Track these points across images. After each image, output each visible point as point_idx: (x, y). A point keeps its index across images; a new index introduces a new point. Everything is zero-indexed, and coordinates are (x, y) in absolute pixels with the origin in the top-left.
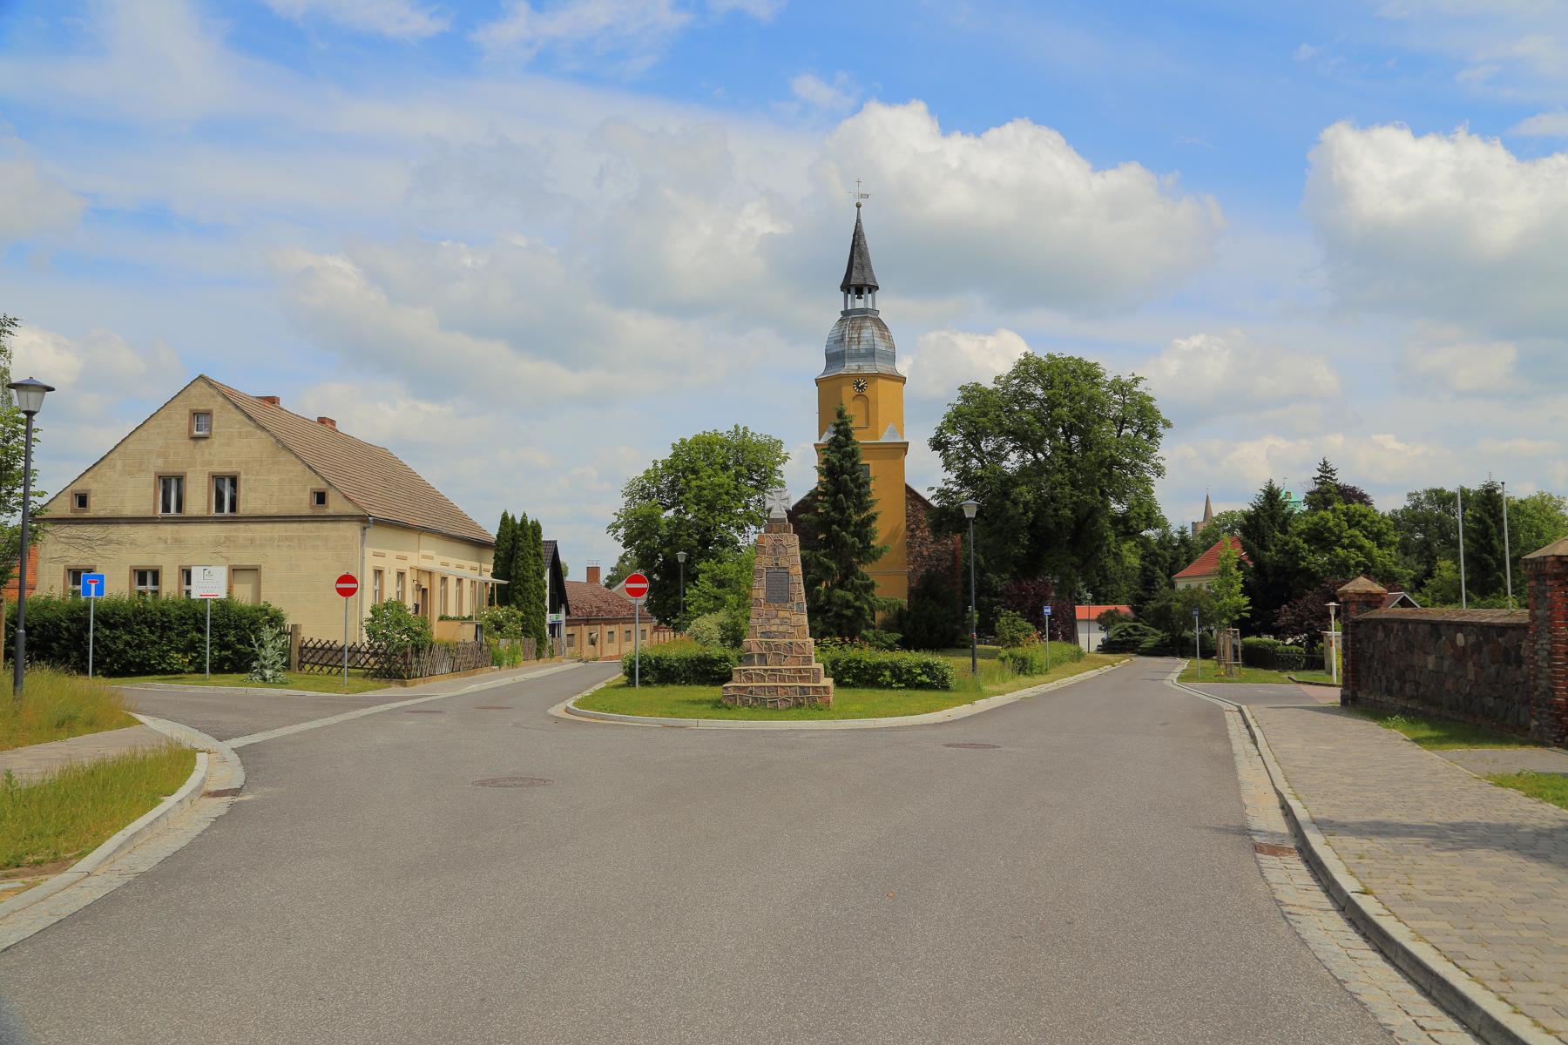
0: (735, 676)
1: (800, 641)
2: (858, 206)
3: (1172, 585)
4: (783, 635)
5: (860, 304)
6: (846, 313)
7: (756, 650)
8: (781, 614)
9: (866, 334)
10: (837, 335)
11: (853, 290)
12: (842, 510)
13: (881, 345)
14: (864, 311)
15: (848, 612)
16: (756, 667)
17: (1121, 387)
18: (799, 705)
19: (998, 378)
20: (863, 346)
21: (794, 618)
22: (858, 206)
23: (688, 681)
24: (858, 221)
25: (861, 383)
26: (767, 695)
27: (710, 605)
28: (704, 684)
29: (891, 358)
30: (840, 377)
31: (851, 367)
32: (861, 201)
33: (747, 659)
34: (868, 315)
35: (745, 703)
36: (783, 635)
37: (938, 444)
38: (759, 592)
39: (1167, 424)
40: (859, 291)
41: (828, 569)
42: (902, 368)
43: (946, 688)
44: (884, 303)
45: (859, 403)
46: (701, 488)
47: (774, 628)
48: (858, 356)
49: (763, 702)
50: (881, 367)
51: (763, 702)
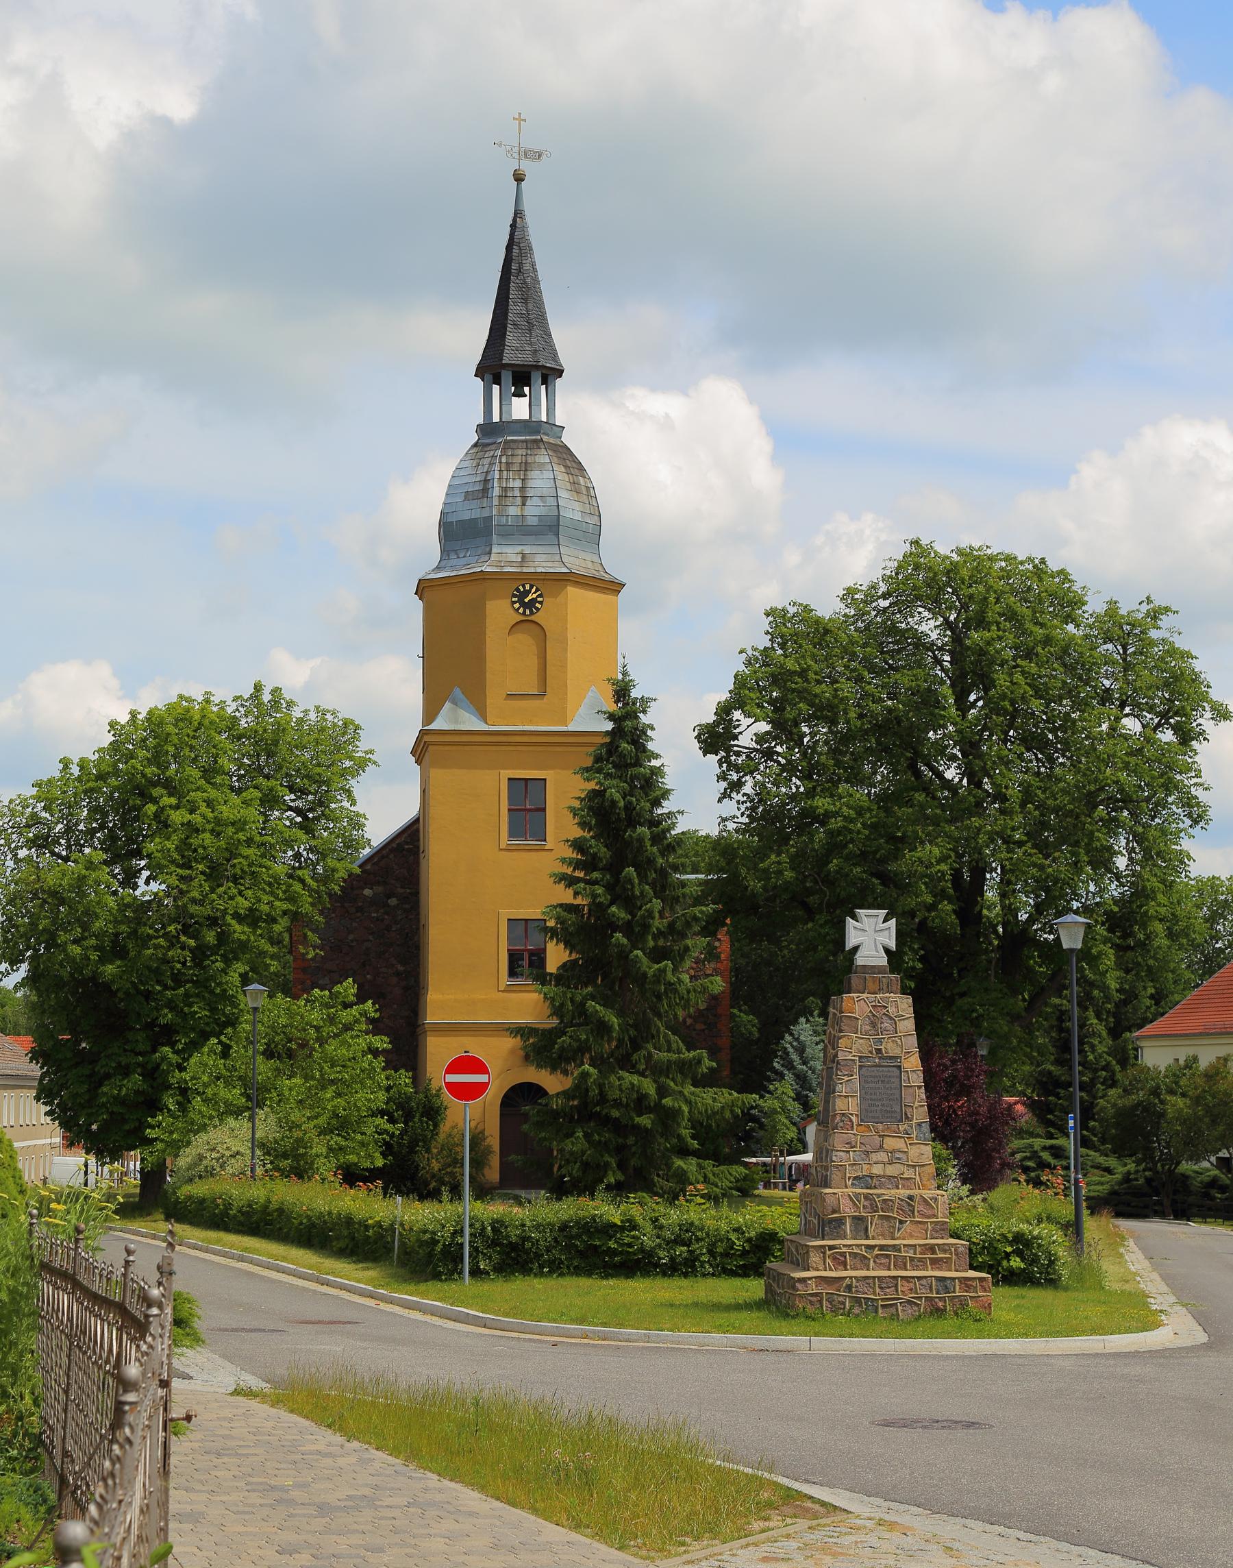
0: (815, 1258)
1: (927, 1194)
2: (519, 178)
3: (1126, 1057)
4: (895, 1181)
5: (520, 408)
6: (488, 430)
7: (848, 1210)
8: (890, 1143)
9: (540, 481)
10: (473, 481)
11: (507, 377)
12: (629, 903)
13: (572, 510)
14: (530, 426)
15: (645, 1121)
16: (848, 1242)
17: (1115, 627)
18: (938, 1312)
19: (850, 592)
20: (533, 510)
21: (914, 1152)
22: (519, 178)
23: (555, 1269)
24: (518, 214)
26: (878, 1294)
28: (589, 1274)
29: (592, 536)
30: (482, 577)
31: (505, 556)
32: (527, 166)
33: (829, 1225)
34: (539, 435)
35: (837, 1308)
36: (895, 1181)
37: (715, 738)
38: (847, 1101)
39: (1221, 714)
40: (521, 379)
41: (602, 1028)
43: (1052, 1282)
44: (576, 410)
45: (525, 641)
47: (877, 1170)
49: (871, 1306)
50: (574, 559)
51: (871, 1306)
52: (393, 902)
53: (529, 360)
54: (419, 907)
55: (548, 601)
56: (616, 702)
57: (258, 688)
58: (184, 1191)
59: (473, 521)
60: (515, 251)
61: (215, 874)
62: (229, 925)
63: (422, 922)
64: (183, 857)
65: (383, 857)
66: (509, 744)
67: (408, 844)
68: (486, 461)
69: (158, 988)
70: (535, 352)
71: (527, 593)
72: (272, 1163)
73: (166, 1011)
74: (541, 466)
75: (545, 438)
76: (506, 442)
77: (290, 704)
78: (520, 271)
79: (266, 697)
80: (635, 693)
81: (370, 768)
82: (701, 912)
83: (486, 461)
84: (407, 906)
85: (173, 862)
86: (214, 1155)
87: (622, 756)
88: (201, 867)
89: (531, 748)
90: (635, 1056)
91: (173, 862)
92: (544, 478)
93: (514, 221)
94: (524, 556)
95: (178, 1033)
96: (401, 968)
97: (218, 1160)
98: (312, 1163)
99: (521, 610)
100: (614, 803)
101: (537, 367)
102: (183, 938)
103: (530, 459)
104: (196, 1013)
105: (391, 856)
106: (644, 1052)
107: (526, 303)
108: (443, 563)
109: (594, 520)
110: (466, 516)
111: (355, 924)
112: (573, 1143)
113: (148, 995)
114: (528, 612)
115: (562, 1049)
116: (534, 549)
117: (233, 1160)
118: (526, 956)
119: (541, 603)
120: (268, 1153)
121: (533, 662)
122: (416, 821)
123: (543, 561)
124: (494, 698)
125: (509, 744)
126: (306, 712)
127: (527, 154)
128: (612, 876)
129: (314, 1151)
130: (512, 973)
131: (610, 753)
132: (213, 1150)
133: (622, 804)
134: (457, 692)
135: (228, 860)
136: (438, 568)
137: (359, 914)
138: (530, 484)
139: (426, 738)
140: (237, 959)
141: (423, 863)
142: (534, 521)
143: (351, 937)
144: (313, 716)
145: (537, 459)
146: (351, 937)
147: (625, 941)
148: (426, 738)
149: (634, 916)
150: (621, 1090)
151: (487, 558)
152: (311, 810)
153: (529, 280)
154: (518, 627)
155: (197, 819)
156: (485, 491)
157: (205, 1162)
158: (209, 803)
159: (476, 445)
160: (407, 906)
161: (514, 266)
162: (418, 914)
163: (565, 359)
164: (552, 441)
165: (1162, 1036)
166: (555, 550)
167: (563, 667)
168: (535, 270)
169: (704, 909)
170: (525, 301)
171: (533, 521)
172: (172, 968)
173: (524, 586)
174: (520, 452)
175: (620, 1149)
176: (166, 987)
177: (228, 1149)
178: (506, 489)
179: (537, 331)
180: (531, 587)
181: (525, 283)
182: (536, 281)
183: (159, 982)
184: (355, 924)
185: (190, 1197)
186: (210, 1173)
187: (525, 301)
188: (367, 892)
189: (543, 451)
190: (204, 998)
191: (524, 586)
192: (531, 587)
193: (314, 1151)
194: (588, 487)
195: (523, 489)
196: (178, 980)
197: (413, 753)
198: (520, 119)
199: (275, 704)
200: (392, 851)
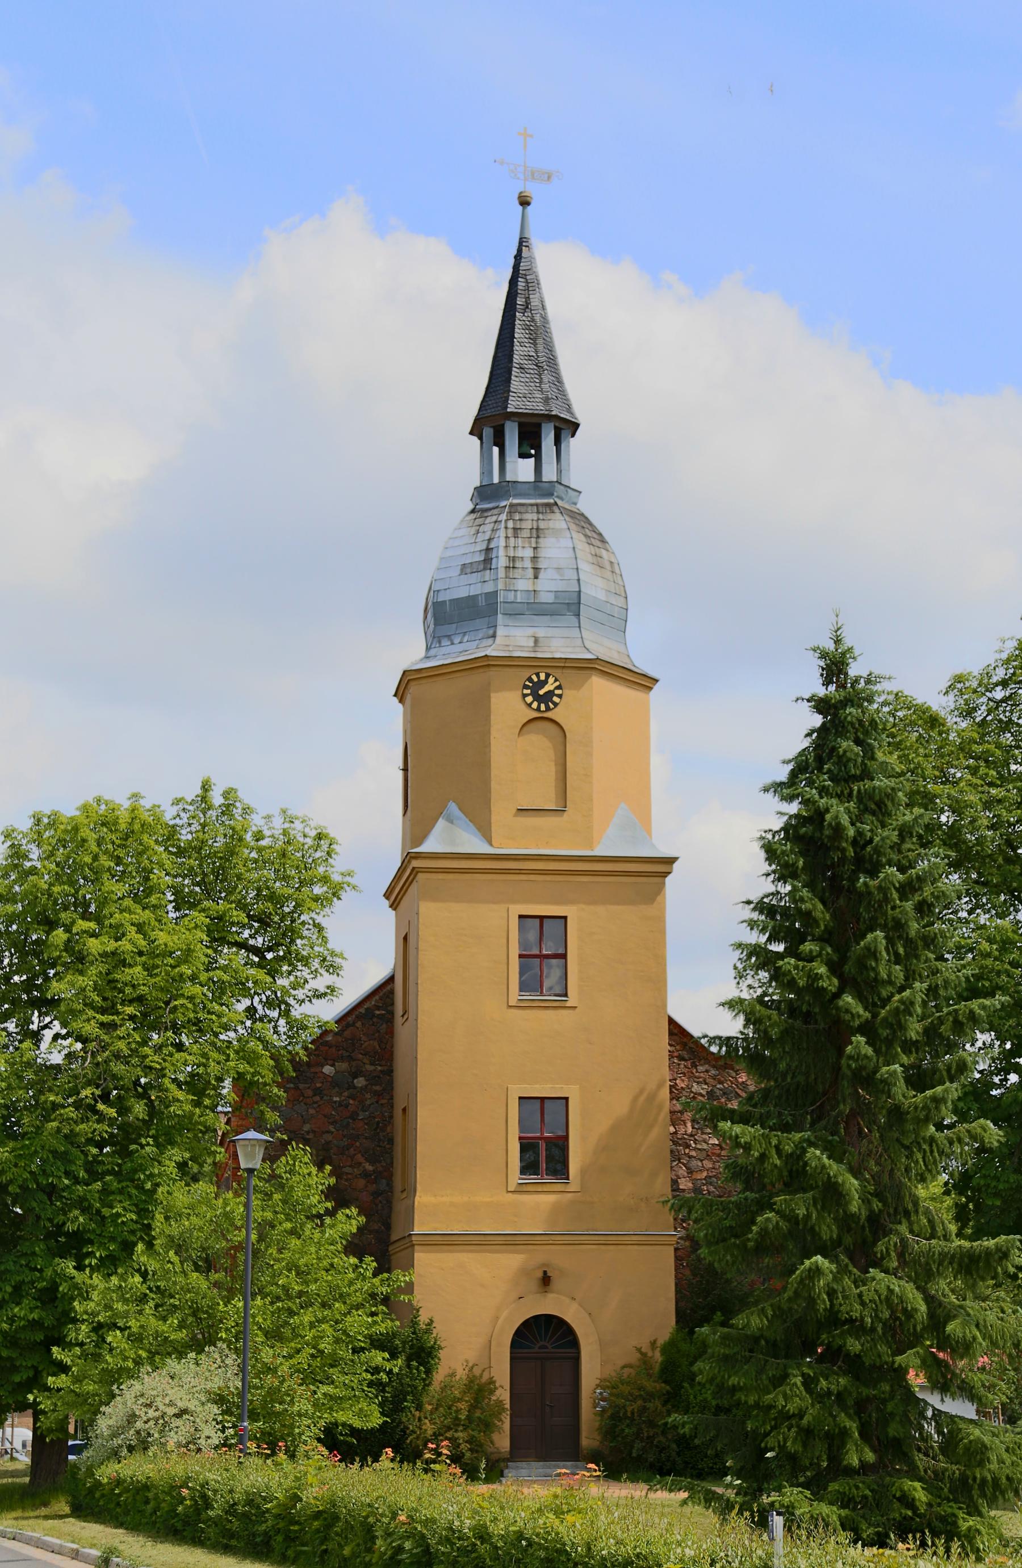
2: (524, 202)
12: (867, 987)
13: (595, 588)
20: (548, 586)
22: (524, 202)
24: (523, 242)
25: (542, 685)
27: (171, 1329)
29: (618, 622)
30: (486, 663)
31: (513, 638)
32: (532, 190)
42: (640, 652)
45: (539, 742)
46: (117, 960)
48: (535, 609)
50: (597, 644)
52: (360, 1082)
53: (540, 408)
54: (392, 1089)
55: (567, 693)
56: (827, 683)
57: (206, 787)
58: (106, 1473)
59: (472, 599)
60: (521, 284)
61: (146, 1022)
62: (167, 1090)
63: (399, 1104)
64: (105, 999)
65: (348, 1026)
67: (379, 1013)
68: (488, 528)
69: (66, 1182)
70: (546, 400)
71: (543, 683)
72: (234, 1426)
73: (76, 1212)
74: (557, 533)
75: (559, 502)
76: (511, 505)
77: (247, 810)
78: (527, 305)
79: (217, 799)
80: (854, 670)
81: (346, 895)
82: (984, 1007)
83: (488, 528)
84: (377, 1088)
85: (91, 1005)
87: (843, 760)
88: (129, 1010)
90: (880, 1247)
91: (91, 1005)
92: (560, 546)
93: (520, 251)
94: (536, 641)
95: (91, 1242)
96: (369, 1168)
97: (157, 1420)
98: (292, 1426)
99: (535, 705)
100: (838, 829)
101: (549, 418)
102: (101, 1106)
103: (542, 525)
104: (118, 1215)
105: (359, 1024)
106: (895, 1239)
107: (535, 344)
108: (432, 652)
109: (619, 602)
110: (463, 593)
111: (312, 1111)
112: (786, 1397)
113: (51, 1192)
114: (543, 707)
115: (764, 1233)
116: (550, 632)
117: (178, 1422)
118: (542, 1146)
119: (560, 696)
120: (227, 1412)
121: (550, 770)
122: (391, 979)
123: (560, 642)
124: (501, 814)
126: (268, 818)
127: (533, 175)
128: (836, 950)
129: (296, 1408)
130: (529, 1167)
131: (820, 761)
132: (149, 1406)
133: (851, 832)
134: (453, 807)
135: (167, 1003)
136: (427, 657)
137: (317, 1098)
138: (542, 553)
139: (415, 863)
140: (172, 1143)
141: (402, 1031)
142: (549, 598)
143: (307, 1127)
144: (278, 823)
145: (551, 524)
146: (307, 1127)
147: (869, 1051)
148: (415, 863)
149: (875, 1016)
150: (863, 1304)
151: (490, 641)
152: (270, 949)
153: (537, 318)
154: (525, 729)
155: (125, 945)
156: (488, 562)
157: (139, 1425)
158: (140, 928)
159: (473, 511)
160: (377, 1088)
161: (520, 301)
162: (392, 1098)
163: (580, 413)
164: (567, 506)
166: (575, 632)
168: (544, 308)
169: (987, 1002)
170: (534, 342)
171: (546, 598)
172: (85, 1154)
173: (538, 675)
174: (529, 516)
175: (860, 1408)
176: (77, 1181)
177: (171, 1404)
178: (514, 559)
179: (546, 377)
180: (548, 676)
181: (533, 320)
182: (545, 319)
183: (67, 1174)
184: (312, 1111)
185: (119, 1482)
186: (143, 1444)
187: (534, 342)
188: (328, 1070)
189: (558, 515)
190: (130, 1197)
191: (538, 675)
192: (548, 676)
193: (296, 1408)
194: (611, 563)
195: (535, 559)
196: (94, 1172)
197: (387, 895)
199: (227, 810)
200: (359, 1017)
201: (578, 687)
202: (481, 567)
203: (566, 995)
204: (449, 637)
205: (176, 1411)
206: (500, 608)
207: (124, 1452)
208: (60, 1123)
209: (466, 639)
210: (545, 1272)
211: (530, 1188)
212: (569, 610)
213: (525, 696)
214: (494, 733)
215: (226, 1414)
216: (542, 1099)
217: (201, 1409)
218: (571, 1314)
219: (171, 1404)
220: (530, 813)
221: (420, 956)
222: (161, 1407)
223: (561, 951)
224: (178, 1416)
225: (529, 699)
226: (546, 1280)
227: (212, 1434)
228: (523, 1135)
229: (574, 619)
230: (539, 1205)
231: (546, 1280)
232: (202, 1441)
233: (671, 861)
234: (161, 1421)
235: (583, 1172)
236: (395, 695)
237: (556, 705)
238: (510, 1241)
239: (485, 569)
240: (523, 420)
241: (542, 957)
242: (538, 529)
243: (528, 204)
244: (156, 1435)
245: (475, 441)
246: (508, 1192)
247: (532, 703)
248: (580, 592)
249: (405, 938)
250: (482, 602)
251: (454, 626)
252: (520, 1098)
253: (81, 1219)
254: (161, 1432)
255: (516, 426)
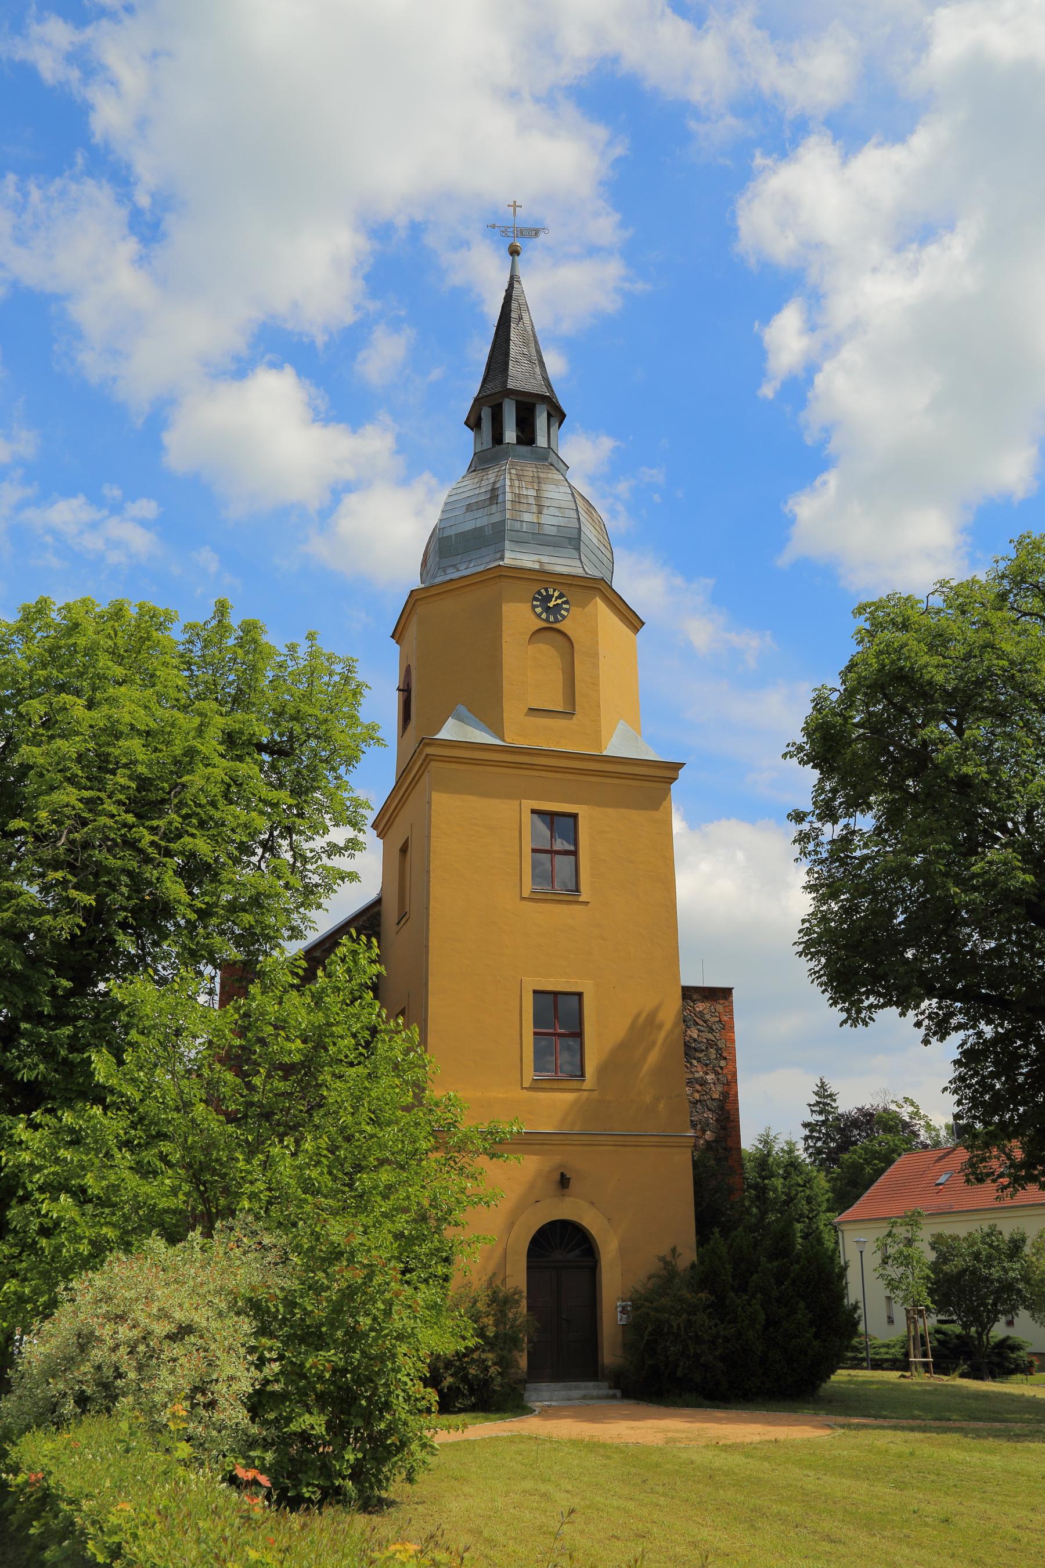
2: (514, 252)
22: (514, 252)
27: (166, 1190)
45: (547, 653)
48: (538, 539)
66: (532, 766)
85: (72, 780)
86: (124, 1332)
89: (559, 776)
103: (542, 475)
110: (469, 526)
114: (552, 619)
117: (177, 1350)
121: (557, 677)
122: (378, 902)
123: (562, 564)
124: (513, 713)
125: (532, 766)
132: (120, 1318)
142: (553, 531)
148: (429, 750)
157: (97, 1354)
165: (854, 1221)
167: (595, 683)
173: (546, 590)
177: (164, 1315)
191: (546, 590)
195: (538, 497)
198: (515, 206)
201: (583, 605)
202: (488, 503)
203: (578, 890)
204: (454, 566)
205: (171, 1328)
206: (508, 535)
207: (69, 1407)
208: (15, 913)
209: (472, 565)
210: (562, 1175)
211: (545, 1085)
212: (570, 544)
213: (534, 607)
214: (505, 638)
215: (263, 1335)
216: (556, 994)
217: (219, 1324)
218: (590, 1220)
219: (164, 1315)
220: (541, 713)
221: (432, 843)
222: (144, 1320)
223: (572, 848)
224: (171, 1337)
225: (539, 610)
226: (564, 1182)
227: (240, 1372)
228: (537, 1030)
229: (575, 553)
230: (553, 1108)
231: (564, 1182)
232: (221, 1388)
233: (678, 766)
234: (141, 1348)
235: (603, 1071)
236: (392, 637)
237: (564, 617)
238: (528, 1142)
239: (491, 504)
240: (520, 399)
241: (552, 852)
242: (538, 477)
243: (518, 254)
244: (132, 1375)
245: (469, 434)
246: (522, 1088)
247: (541, 613)
248: (580, 528)
249: (404, 850)
250: (489, 532)
251: (459, 557)
252: (535, 992)
253: (42, 1066)
254: (140, 1368)
255: (513, 403)
